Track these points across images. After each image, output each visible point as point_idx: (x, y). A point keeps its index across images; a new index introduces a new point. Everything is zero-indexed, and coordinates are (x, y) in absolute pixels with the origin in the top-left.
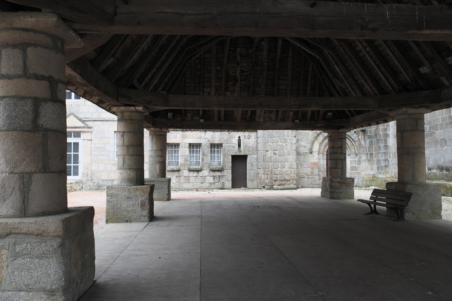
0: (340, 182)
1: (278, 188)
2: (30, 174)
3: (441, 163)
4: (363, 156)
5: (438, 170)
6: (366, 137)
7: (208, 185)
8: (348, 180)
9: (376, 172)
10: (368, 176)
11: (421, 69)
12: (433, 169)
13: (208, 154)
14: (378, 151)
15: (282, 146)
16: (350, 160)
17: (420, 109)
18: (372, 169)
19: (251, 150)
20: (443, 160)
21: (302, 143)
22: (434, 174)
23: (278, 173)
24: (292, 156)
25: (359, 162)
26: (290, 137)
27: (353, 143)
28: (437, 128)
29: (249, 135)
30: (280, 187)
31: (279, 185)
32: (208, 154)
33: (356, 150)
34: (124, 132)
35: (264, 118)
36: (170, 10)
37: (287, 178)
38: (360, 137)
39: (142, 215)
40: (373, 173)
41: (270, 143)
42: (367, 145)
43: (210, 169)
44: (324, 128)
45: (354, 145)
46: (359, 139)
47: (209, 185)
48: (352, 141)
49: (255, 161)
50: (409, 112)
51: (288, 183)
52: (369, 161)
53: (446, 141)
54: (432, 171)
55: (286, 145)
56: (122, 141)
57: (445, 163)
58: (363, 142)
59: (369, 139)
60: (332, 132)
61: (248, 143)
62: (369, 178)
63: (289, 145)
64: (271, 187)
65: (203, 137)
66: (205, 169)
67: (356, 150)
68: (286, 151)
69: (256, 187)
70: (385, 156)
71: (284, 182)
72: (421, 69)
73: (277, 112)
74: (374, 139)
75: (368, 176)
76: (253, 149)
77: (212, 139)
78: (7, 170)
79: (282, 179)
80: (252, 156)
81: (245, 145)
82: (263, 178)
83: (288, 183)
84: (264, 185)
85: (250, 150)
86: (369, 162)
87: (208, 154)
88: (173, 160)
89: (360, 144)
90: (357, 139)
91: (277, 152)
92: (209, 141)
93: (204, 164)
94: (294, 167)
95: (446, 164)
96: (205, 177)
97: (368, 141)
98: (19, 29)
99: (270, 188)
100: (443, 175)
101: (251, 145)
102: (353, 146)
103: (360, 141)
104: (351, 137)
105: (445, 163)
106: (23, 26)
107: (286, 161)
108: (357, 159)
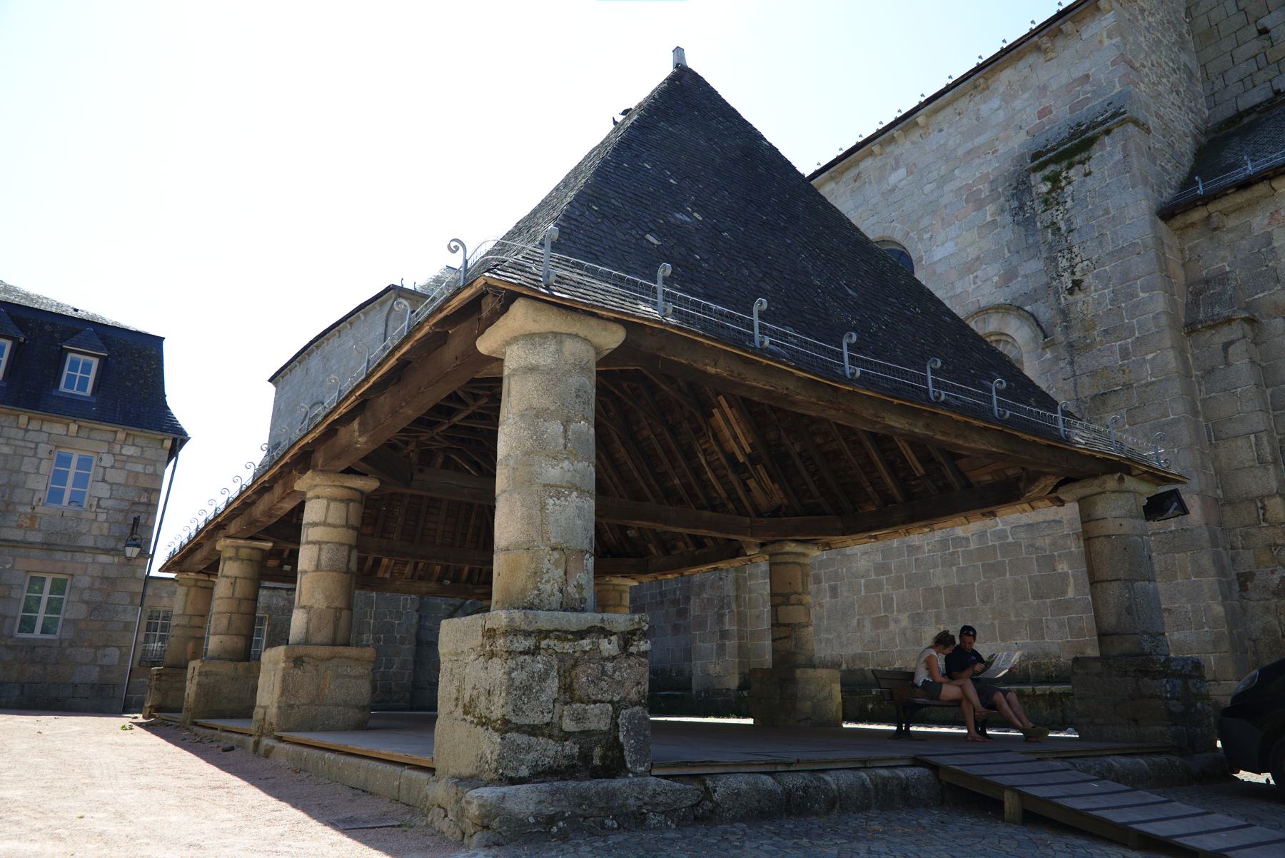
2: (341, 609)
11: (628, 532)
15: (393, 625)
17: (626, 579)
21: (427, 624)
28: (644, 608)
35: (392, 573)
36: (454, 482)
50: (613, 582)
55: (399, 624)
70: (418, 796)
72: (628, 532)
73: (417, 564)
98: (346, 487)
106: (352, 486)
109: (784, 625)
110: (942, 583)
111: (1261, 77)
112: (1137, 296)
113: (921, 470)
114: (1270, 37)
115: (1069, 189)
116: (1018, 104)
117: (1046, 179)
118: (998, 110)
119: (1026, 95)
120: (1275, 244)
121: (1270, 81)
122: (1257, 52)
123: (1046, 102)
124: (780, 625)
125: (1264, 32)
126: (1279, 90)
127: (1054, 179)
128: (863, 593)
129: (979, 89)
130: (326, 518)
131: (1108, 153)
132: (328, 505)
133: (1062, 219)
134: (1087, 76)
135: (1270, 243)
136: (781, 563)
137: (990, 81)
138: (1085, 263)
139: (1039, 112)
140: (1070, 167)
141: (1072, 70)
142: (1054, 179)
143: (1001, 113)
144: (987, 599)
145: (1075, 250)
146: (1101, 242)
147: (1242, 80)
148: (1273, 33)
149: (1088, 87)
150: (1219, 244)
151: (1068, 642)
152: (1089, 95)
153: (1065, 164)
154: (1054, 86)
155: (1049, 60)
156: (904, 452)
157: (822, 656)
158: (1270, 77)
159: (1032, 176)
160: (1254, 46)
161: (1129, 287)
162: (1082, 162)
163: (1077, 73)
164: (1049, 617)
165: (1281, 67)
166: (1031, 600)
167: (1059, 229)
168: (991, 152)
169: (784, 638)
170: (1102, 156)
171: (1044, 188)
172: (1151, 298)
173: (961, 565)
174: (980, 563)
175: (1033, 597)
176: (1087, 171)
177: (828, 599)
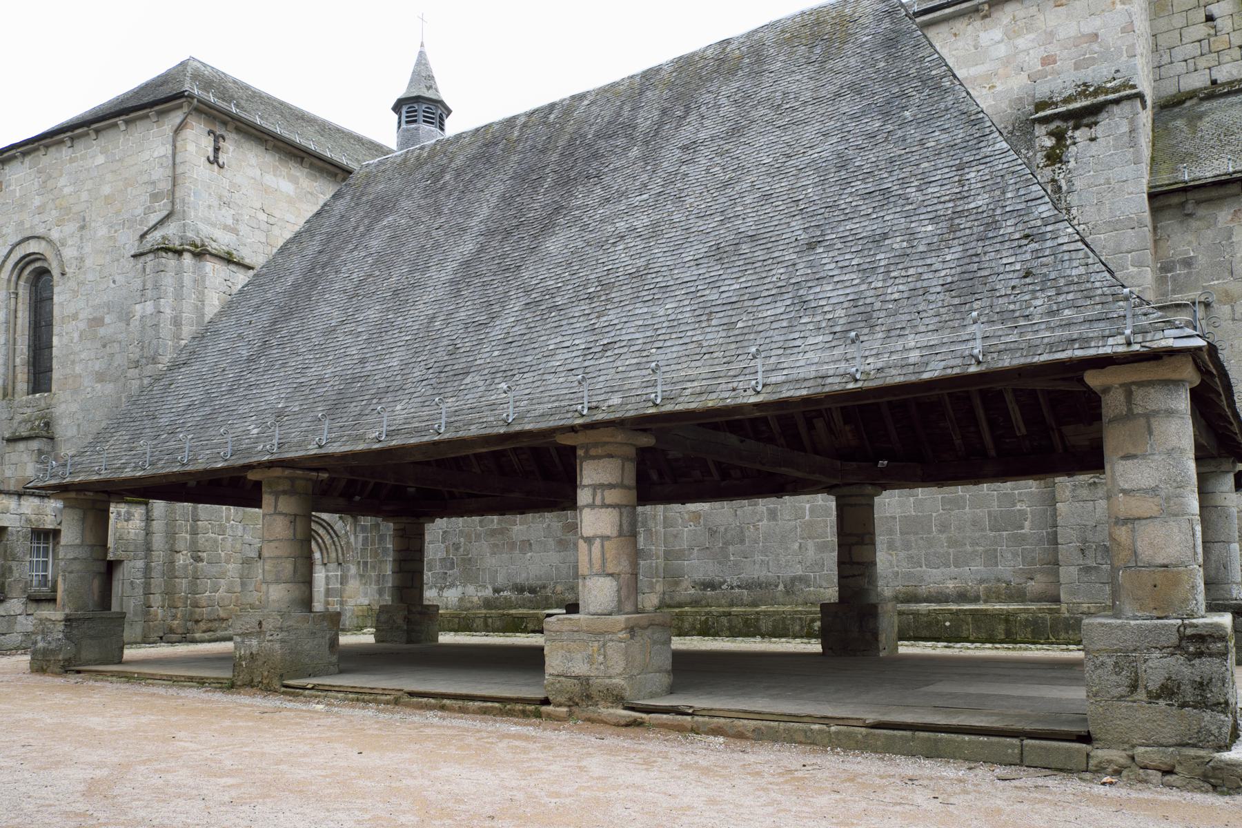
0: (420, 613)
1: (203, 639)
3: (519, 580)
4: (352, 566)
5: (513, 593)
6: (358, 529)
7: (20, 638)
8: (431, 609)
9: (374, 600)
10: (360, 608)
12: (503, 591)
13: (24, 556)
14: (383, 556)
15: (216, 541)
16: (324, 576)
18: (366, 594)
19: (131, 548)
20: (524, 575)
22: (505, 598)
23: (205, 604)
24: (233, 565)
25: (344, 580)
26: (232, 522)
27: (336, 539)
29: (128, 512)
30: (206, 636)
31: (204, 632)
32: (25, 555)
33: (340, 555)
34: (295, 515)
37: (222, 614)
38: (348, 528)
39: (330, 663)
40: (367, 602)
41: (183, 535)
42: (360, 546)
43: (28, 597)
44: (388, 515)
45: (337, 544)
46: (346, 533)
47: (24, 638)
48: (333, 535)
49: (140, 575)
51: (224, 625)
52: (362, 576)
53: (530, 544)
54: (502, 594)
55: (223, 540)
56: (292, 531)
57: (528, 580)
58: (352, 539)
59: (363, 533)
60: (409, 521)
61: (126, 531)
62: (363, 611)
63: (230, 539)
64: (184, 636)
65: (12, 512)
66: (14, 595)
67: (340, 555)
68: (223, 554)
69: (139, 640)
71: (216, 624)
74: (371, 532)
75: (360, 608)
76: (136, 546)
77: (37, 517)
78: (630, 571)
79: (212, 617)
80: (131, 564)
81: (118, 534)
82: (160, 617)
83: (224, 625)
84: (161, 634)
85: (130, 550)
86: (361, 580)
87: (24, 556)
88: (34, 574)
89: (348, 543)
90: (343, 532)
91: (205, 554)
92: (28, 520)
93: (13, 583)
94: (236, 590)
95: (531, 582)
96: (12, 618)
97: (361, 536)
99: (180, 639)
100: (524, 599)
101: (132, 536)
102: (333, 547)
103: (348, 536)
104: (332, 528)
105: (528, 580)
107: (222, 575)
108: (339, 573)
109: (858, 563)
110: (898, 512)
111: (1202, 63)
112: (1128, 269)
113: (1024, 431)
114: (1215, 27)
115: (1073, 149)
116: (1022, 42)
117: (1050, 134)
118: (999, 42)
119: (1032, 36)
120: (1234, 239)
121: (1210, 68)
122: (1202, 37)
123: (1053, 49)
124: (854, 563)
125: (1210, 18)
126: (1216, 80)
127: (1059, 136)
128: (807, 518)
129: (981, 14)
130: (622, 481)
131: (1113, 124)
132: (623, 466)
133: (1063, 178)
134: (1096, 35)
135: (1230, 238)
136: (855, 505)
137: (992, 10)
138: (1083, 226)
139: (1043, 59)
140: (1076, 128)
141: (1082, 23)
142: (1059, 136)
143: (1002, 48)
144: (944, 528)
145: (1074, 211)
146: (1099, 210)
147: (1186, 61)
148: (1218, 22)
149: (1096, 47)
150: (1187, 229)
151: (1020, 569)
152: (1096, 55)
153: (1071, 124)
154: (1062, 34)
155: (1059, 6)
156: (1011, 413)
157: (756, 576)
158: (1210, 66)
159: (1037, 126)
160: (1202, 30)
161: (1121, 258)
162: (1090, 126)
163: (1087, 29)
164: (1005, 548)
165: (1221, 58)
166: (988, 532)
167: (1060, 188)
168: (988, 86)
169: (859, 575)
170: (1109, 124)
171: (1049, 142)
172: (1139, 273)
173: (920, 496)
174: (940, 496)
175: (990, 529)
176: (1093, 136)
177: (765, 521)
